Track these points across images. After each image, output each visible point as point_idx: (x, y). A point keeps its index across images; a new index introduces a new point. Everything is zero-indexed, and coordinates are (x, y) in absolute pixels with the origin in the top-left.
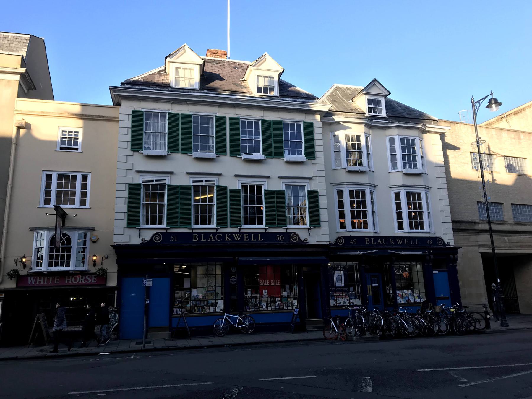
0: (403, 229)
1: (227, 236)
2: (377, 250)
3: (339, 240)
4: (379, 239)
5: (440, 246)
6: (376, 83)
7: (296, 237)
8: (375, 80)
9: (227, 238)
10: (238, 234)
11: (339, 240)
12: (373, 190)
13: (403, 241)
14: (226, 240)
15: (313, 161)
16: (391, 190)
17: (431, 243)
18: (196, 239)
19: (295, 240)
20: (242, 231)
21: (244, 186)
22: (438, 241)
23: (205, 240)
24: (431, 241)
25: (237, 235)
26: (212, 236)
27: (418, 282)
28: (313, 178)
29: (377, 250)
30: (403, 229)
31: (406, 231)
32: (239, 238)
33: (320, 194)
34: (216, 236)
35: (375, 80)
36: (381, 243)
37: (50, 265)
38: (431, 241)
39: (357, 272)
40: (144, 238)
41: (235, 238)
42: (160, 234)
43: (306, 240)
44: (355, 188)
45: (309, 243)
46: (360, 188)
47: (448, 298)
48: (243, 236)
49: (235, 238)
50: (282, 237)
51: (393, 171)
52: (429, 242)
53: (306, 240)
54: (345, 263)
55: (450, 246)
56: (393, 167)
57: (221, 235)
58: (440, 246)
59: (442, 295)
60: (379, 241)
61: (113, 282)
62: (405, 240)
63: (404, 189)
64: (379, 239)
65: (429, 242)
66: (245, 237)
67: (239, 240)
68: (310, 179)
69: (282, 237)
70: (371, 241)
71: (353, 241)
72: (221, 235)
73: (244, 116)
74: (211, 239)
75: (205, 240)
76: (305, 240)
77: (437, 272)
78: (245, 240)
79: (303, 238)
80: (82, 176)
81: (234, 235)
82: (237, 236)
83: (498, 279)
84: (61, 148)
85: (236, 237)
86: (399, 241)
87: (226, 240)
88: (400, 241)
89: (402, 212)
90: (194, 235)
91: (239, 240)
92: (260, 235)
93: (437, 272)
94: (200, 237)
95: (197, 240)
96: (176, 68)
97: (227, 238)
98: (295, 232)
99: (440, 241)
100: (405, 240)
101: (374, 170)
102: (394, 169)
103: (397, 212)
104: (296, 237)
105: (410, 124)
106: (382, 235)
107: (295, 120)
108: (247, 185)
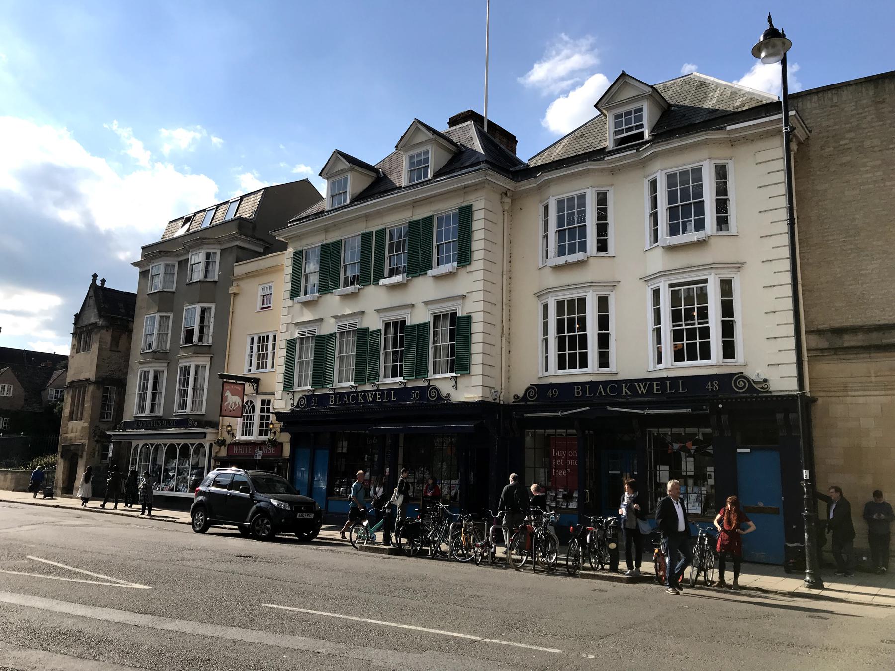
0: (709, 358)
1: (625, 388)
2: (587, 408)
3: (530, 391)
4: (601, 386)
5: (531, 401)
6: (628, 79)
7: (743, 381)
8: (623, 74)
9: (625, 391)
10: (644, 383)
11: (530, 391)
12: (546, 300)
13: (651, 387)
14: (624, 394)
15: (469, 269)
16: (647, 286)
17: (716, 388)
18: (578, 393)
19: (430, 396)
20: (381, 388)
21: (436, 318)
22: (535, 393)
23: (673, 391)
24: (716, 383)
25: (642, 384)
26: (602, 389)
27: (535, 468)
28: (467, 295)
29: (587, 408)
30: (709, 358)
31: (670, 368)
32: (645, 390)
33: (474, 320)
34: (609, 386)
35: (623, 74)
36: (604, 394)
37: (678, 356)
38: (716, 383)
39: (650, 452)
40: (513, 396)
41: (639, 389)
42: (534, 387)
43: (449, 395)
44: (566, 296)
45: (452, 401)
46: (575, 295)
47: (776, 512)
48: (651, 386)
49: (639, 389)
50: (555, 391)
51: (721, 233)
52: (712, 385)
53: (449, 395)
54: (542, 431)
55: (771, 392)
56: (719, 226)
57: (616, 385)
58: (531, 401)
59: (761, 504)
60: (600, 389)
61: (287, 452)
62: (655, 386)
63: (593, 291)
64: (601, 386)
65: (712, 385)
66: (378, 396)
67: (645, 392)
68: (464, 297)
69: (555, 391)
70: (584, 390)
71: (552, 393)
72: (616, 385)
73: (397, 222)
74: (600, 393)
75: (673, 391)
76: (446, 397)
77: (748, 451)
78: (655, 392)
79: (444, 393)
80: (598, 297)
81: (636, 384)
82: (642, 387)
83: (804, 471)
84: (262, 308)
85: (640, 388)
86: (640, 388)
87: (624, 394)
88: (642, 387)
89: (608, 334)
90: (576, 387)
91: (645, 392)
92: (670, 383)
93: (748, 451)
94: (584, 390)
95: (580, 395)
96: (594, 106)
97: (625, 391)
98: (742, 373)
99: (741, 383)
100: (655, 386)
101: (615, 253)
102: (721, 230)
103: (599, 333)
104: (743, 381)
105: (678, 142)
106: (620, 377)
107: (449, 208)
108: (447, 312)
